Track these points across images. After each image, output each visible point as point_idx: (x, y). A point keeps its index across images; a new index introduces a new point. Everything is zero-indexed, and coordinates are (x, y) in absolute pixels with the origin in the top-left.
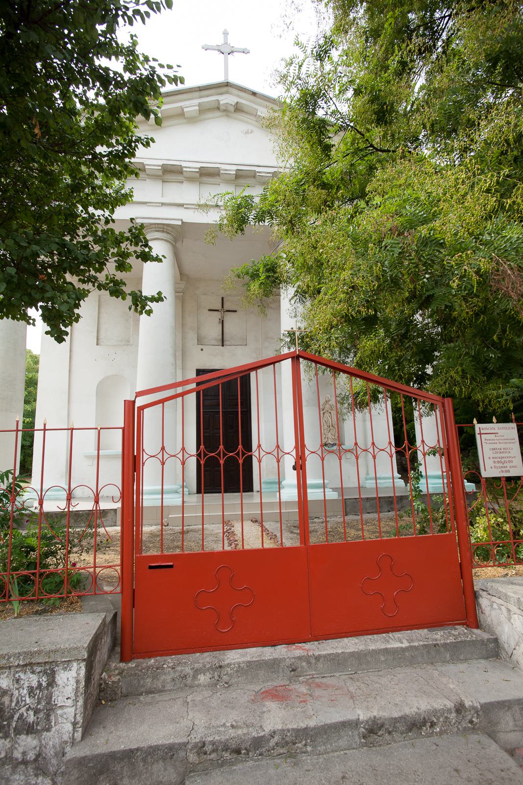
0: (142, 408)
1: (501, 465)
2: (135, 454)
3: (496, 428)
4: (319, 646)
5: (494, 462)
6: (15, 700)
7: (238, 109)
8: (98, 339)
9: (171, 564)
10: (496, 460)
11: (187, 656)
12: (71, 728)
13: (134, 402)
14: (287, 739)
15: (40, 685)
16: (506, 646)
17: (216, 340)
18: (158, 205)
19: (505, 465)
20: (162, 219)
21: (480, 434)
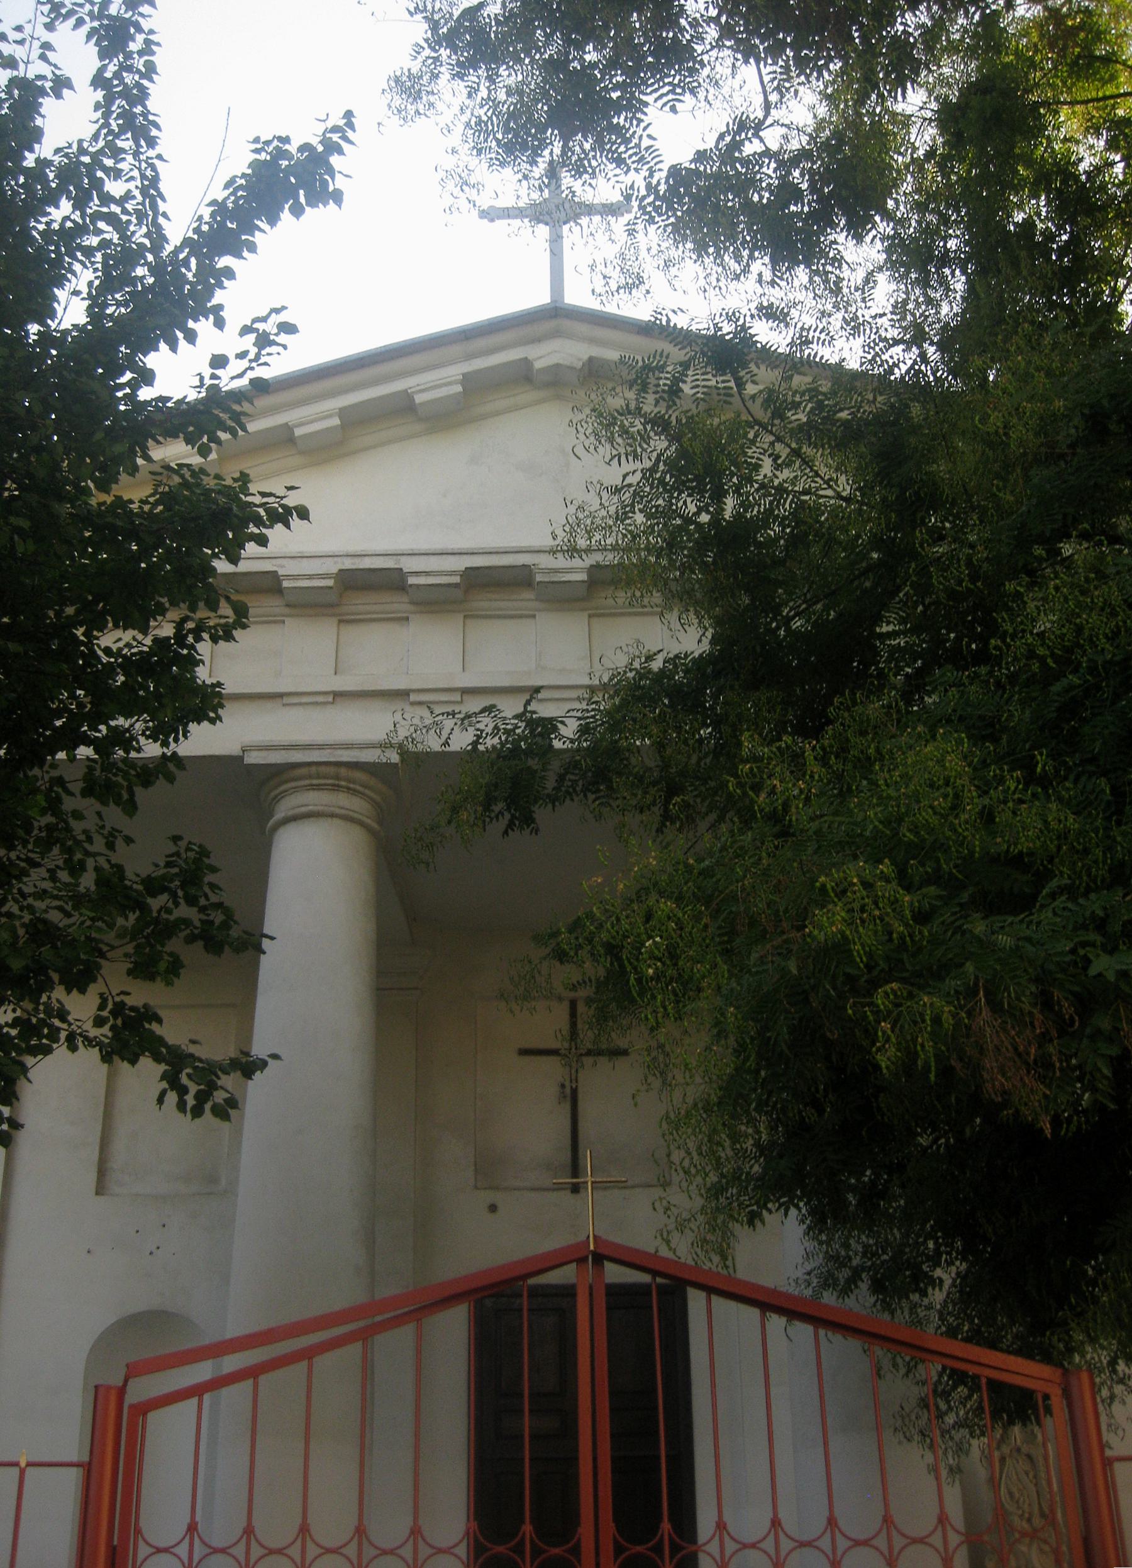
2: (115, 1543)
13: (122, 1391)
18: (321, 699)
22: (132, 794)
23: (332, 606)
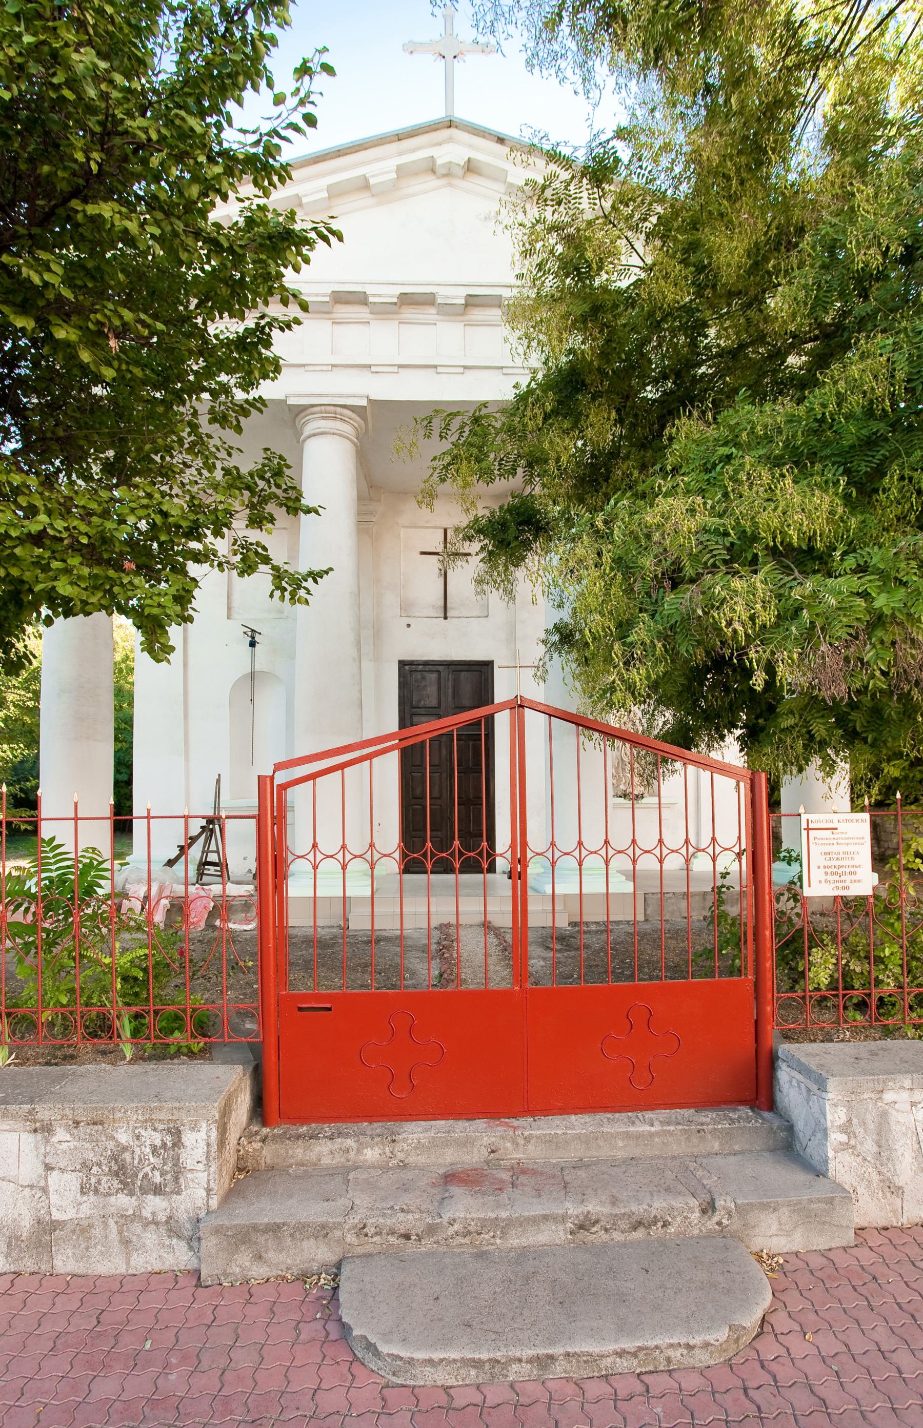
0: (284, 787)
1: (837, 878)
3: (835, 821)
4: (533, 1124)
5: (826, 873)
6: (137, 1157)
7: (470, 168)
8: (229, 609)
9: (329, 1006)
10: (829, 871)
11: (350, 1125)
12: (204, 1194)
14: (470, 1228)
15: (164, 1145)
16: (801, 1135)
17: (433, 607)
18: (325, 368)
19: (843, 878)
20: (333, 396)
21: (808, 829)
22: (238, 421)
23: (328, 313)
